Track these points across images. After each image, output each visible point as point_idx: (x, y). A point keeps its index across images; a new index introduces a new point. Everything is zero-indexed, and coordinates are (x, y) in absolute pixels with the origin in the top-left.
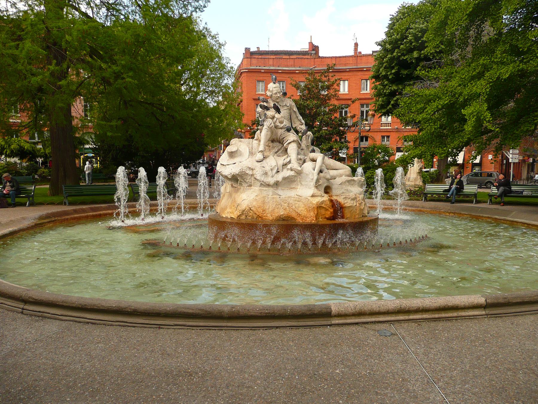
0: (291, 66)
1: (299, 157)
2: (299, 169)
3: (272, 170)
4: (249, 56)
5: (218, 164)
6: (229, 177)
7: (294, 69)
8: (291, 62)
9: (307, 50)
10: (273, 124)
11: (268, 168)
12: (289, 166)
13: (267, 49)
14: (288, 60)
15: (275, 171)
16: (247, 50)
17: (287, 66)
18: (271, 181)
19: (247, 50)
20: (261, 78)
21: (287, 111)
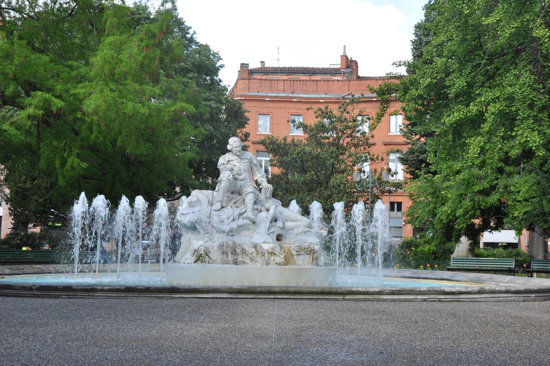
0: (313, 92)
1: (255, 207)
2: (253, 217)
3: (228, 218)
4: (246, 75)
5: (178, 213)
6: (188, 225)
7: (317, 96)
8: (313, 86)
9: (339, 66)
10: (231, 176)
11: (224, 217)
12: (245, 215)
13: (276, 65)
14: (308, 83)
15: (231, 220)
16: (244, 66)
17: (307, 92)
18: (226, 228)
19: (244, 66)
20: (265, 111)
21: (248, 164)
